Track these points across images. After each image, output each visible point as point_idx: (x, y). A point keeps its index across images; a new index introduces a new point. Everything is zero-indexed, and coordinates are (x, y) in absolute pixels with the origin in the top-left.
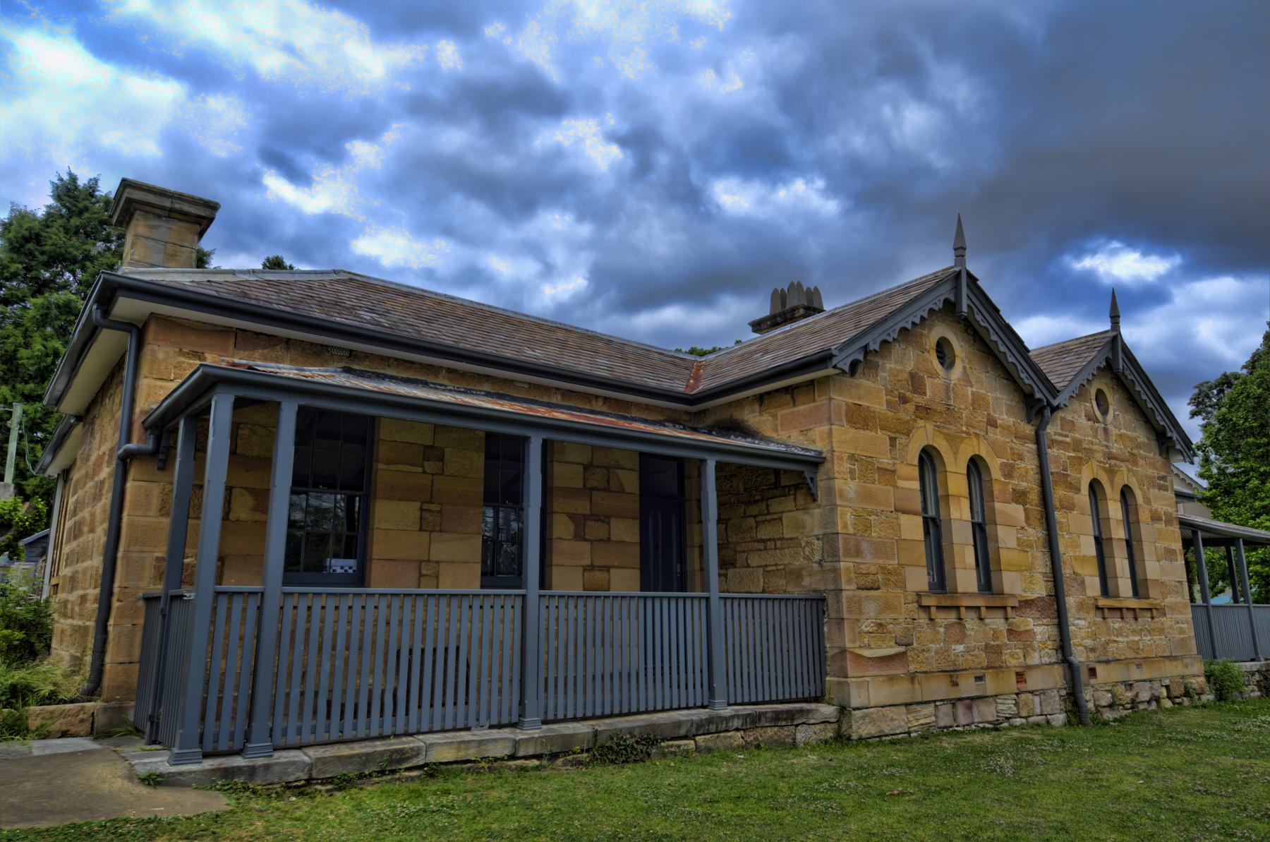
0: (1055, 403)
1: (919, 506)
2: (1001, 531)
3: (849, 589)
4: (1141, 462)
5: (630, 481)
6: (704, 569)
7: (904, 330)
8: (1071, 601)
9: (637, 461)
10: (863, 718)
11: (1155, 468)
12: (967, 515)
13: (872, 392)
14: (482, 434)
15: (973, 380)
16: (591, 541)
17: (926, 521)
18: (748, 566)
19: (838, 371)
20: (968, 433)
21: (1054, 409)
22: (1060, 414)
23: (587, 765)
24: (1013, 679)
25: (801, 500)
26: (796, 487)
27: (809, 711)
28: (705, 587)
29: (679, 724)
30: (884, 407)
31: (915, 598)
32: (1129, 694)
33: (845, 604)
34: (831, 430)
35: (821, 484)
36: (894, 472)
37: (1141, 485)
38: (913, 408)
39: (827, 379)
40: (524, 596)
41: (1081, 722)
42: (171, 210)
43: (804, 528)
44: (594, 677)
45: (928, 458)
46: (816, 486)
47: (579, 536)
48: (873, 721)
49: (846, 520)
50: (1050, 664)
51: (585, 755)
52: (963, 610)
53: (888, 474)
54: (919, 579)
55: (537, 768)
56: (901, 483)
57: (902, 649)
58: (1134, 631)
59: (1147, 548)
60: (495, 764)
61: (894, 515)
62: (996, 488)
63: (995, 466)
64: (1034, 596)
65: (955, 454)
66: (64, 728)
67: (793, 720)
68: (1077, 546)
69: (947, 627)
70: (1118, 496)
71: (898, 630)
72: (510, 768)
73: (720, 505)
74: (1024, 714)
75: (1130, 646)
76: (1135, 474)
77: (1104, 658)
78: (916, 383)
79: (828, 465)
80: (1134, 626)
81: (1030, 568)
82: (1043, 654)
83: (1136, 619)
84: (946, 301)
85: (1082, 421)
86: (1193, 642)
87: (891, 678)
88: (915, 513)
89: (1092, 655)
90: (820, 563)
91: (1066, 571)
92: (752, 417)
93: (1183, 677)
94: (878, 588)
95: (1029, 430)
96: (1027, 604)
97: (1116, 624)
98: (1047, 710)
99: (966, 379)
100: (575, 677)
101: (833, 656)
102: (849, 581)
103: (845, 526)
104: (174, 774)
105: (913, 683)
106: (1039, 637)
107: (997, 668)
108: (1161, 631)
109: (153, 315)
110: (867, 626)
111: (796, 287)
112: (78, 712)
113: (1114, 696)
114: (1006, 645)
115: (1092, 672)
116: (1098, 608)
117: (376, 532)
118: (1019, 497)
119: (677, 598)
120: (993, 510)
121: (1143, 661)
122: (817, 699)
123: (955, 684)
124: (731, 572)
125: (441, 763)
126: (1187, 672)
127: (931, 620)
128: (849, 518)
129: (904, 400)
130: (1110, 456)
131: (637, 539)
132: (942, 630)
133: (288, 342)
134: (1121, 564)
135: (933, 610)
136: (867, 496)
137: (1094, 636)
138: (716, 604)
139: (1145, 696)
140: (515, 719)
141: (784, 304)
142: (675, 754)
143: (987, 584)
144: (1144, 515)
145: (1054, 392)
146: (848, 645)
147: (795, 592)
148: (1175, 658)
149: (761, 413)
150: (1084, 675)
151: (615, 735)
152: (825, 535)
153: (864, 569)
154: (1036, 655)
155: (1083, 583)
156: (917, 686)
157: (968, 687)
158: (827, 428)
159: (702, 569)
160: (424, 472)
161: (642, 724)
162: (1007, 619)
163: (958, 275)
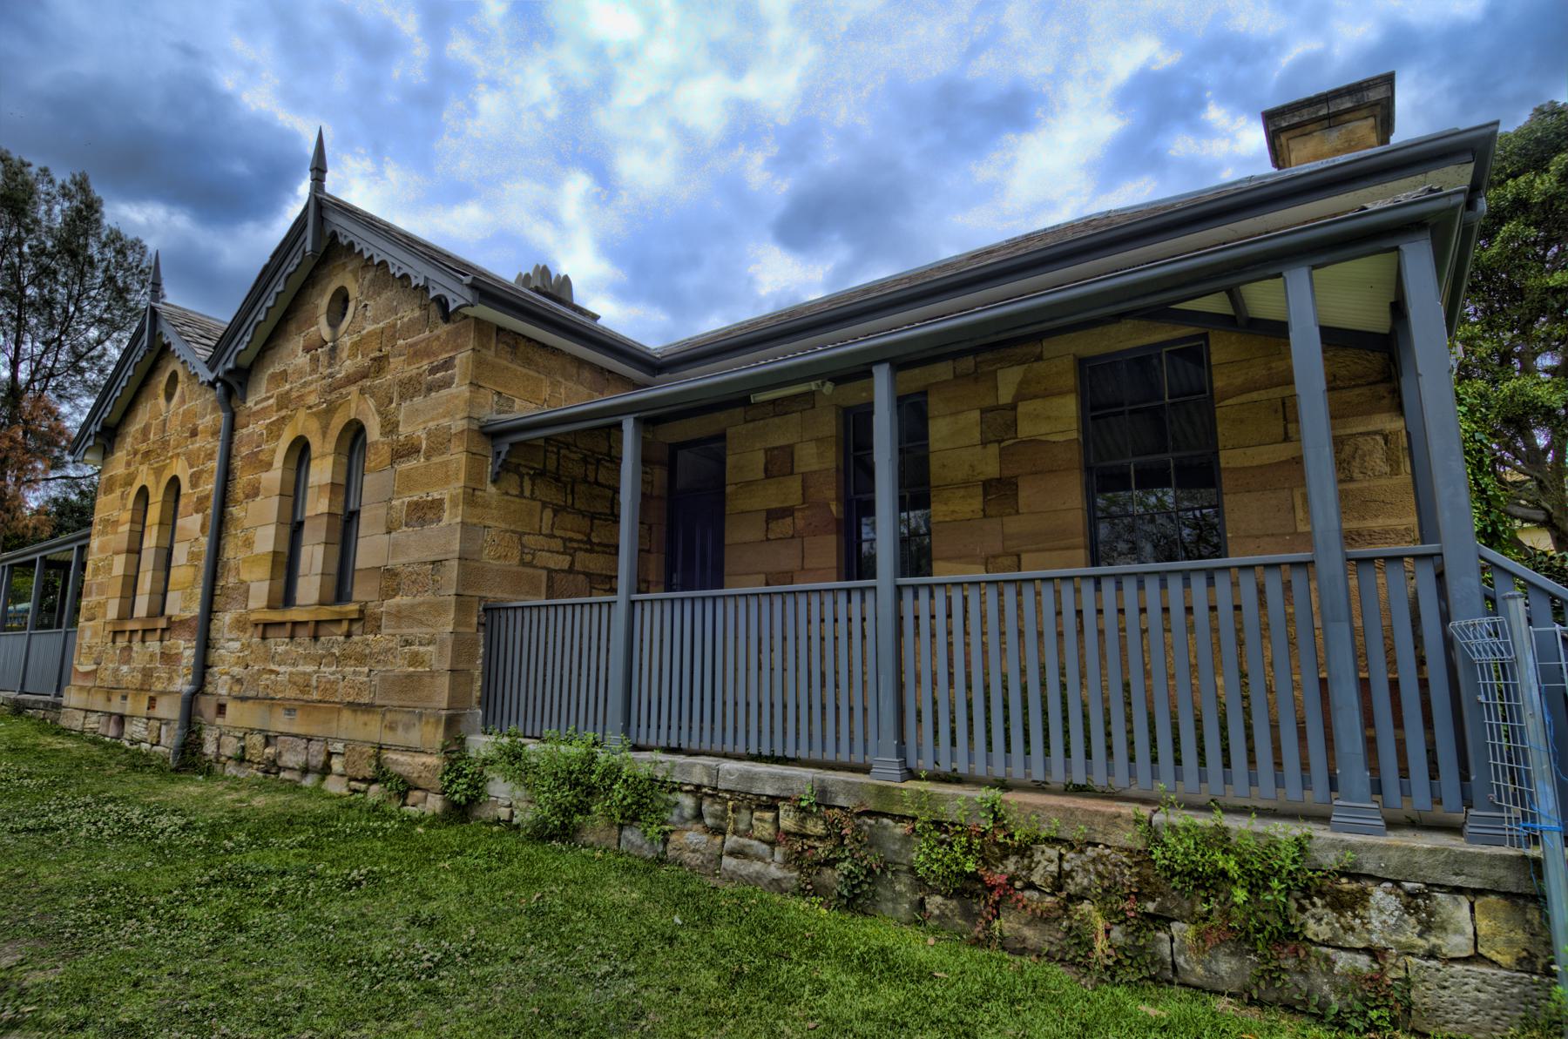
24: (146, 704)
58: (307, 658)
89: (236, 688)
91: (228, 580)
126: (388, 738)
133: (581, 363)
148: (369, 708)
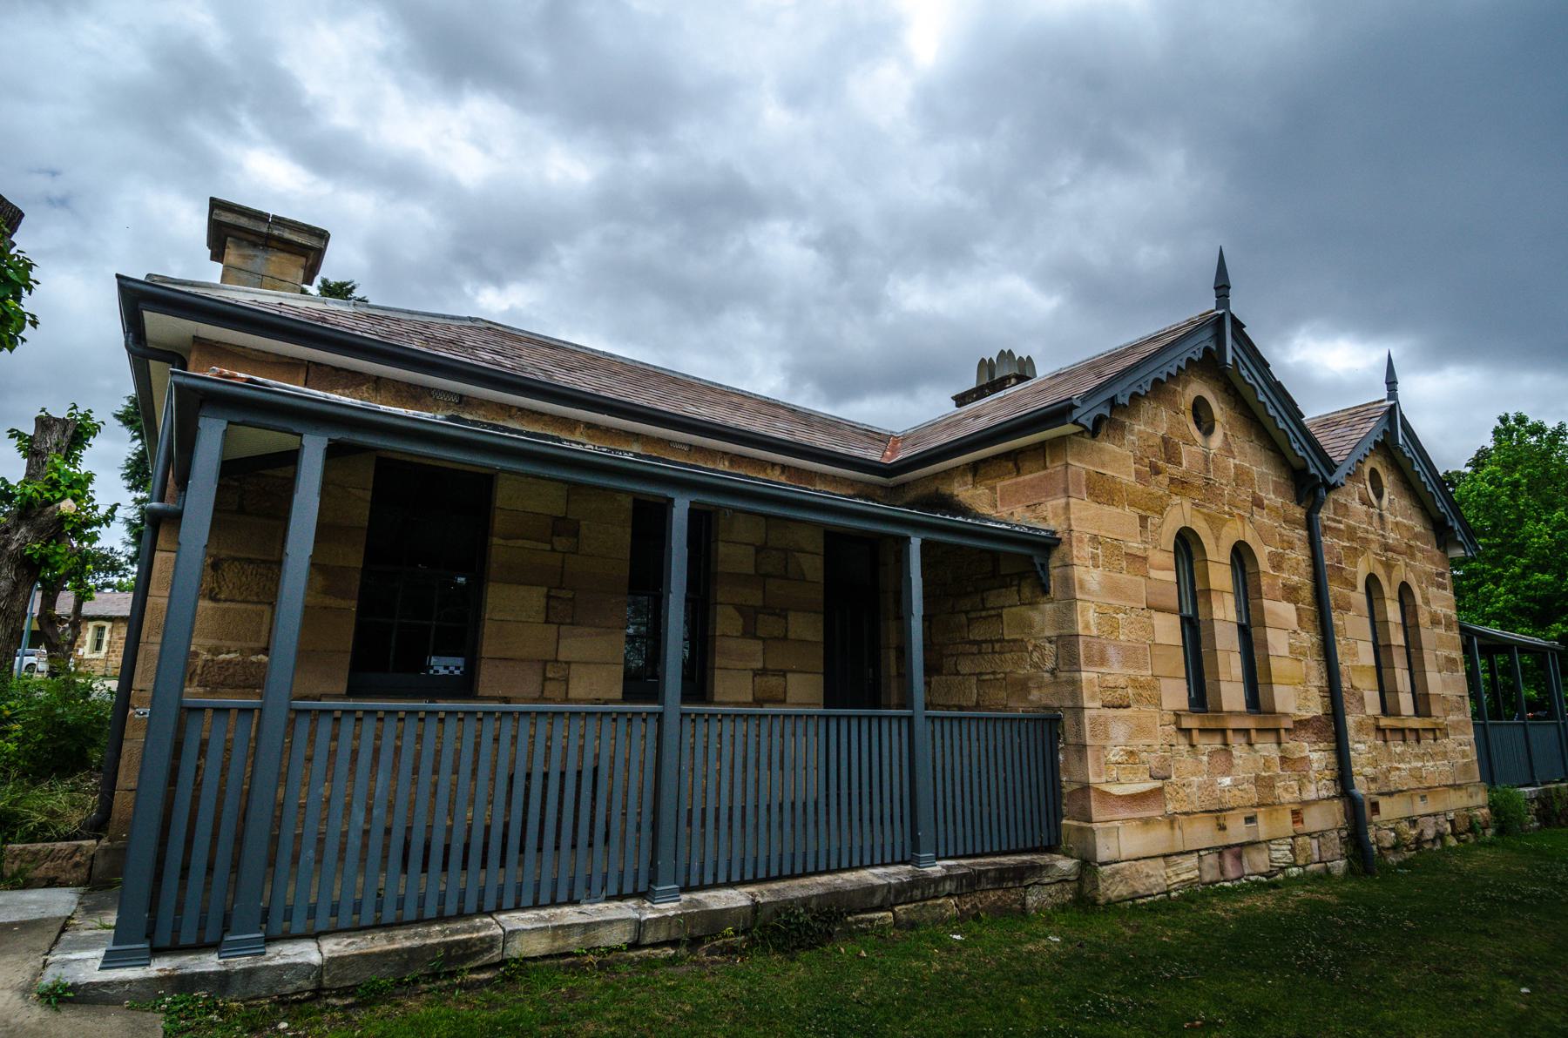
0: (1332, 480)
1: (1175, 604)
2: (1271, 635)
3: (1092, 707)
4: (1419, 555)
5: (813, 567)
6: (905, 676)
7: (1157, 382)
8: (1351, 721)
9: (820, 541)
10: (1112, 875)
11: (1434, 563)
12: (1232, 615)
13: (1117, 459)
14: (627, 502)
15: (1236, 451)
16: (764, 640)
17: (1184, 620)
18: (958, 673)
19: (1077, 429)
20: (1231, 515)
21: (1331, 488)
22: (1333, 496)
23: (742, 953)
24: (1289, 818)
25: (1027, 592)
26: (1021, 576)
27: (1043, 867)
28: (906, 701)
29: (871, 890)
30: (1133, 478)
31: (1173, 718)
32: (1413, 832)
33: (1087, 728)
34: (1068, 504)
35: (1055, 573)
36: (1145, 559)
37: (1419, 582)
38: (1167, 481)
39: (1061, 442)
40: (661, 714)
41: (1368, 871)
42: (269, 237)
43: (1031, 627)
44: (769, 807)
45: (1186, 544)
46: (1047, 574)
47: (749, 633)
48: (1125, 880)
49: (1087, 619)
50: (1328, 798)
51: (741, 938)
52: (1230, 733)
53: (1138, 561)
54: (1176, 694)
55: (670, 961)
56: (1154, 574)
57: (1158, 784)
58: (1417, 757)
59: (1428, 656)
60: (609, 958)
61: (1146, 613)
62: (1265, 582)
63: (1262, 553)
64: (1309, 715)
65: (1217, 539)
66: (51, 874)
67: (1021, 879)
68: (1355, 654)
69: (1211, 755)
70: (1396, 596)
71: (1153, 760)
72: (631, 962)
73: (926, 597)
74: (1301, 862)
75: (1416, 774)
76: (1413, 569)
77: (1385, 790)
78: (1170, 450)
79: (1063, 548)
80: (1416, 750)
81: (1305, 681)
82: (1319, 786)
83: (1418, 741)
84: (1207, 350)
85: (1356, 505)
86: (1476, 766)
87: (1147, 822)
88: (1171, 611)
89: (1373, 786)
90: (1052, 672)
92: (963, 491)
93: (1468, 809)
94: (1128, 706)
95: (1299, 513)
96: (1302, 724)
97: (1398, 748)
98: (1327, 855)
99: (1227, 449)
100: (744, 808)
101: (1070, 794)
102: (1093, 697)
103: (1087, 627)
104: (107, 985)
105: (1172, 828)
106: (1315, 765)
107: (1269, 805)
108: (1445, 755)
109: (198, 341)
110: (1115, 755)
111: (1006, 356)
112: (73, 854)
113: (1398, 835)
114: (1279, 776)
115: (1375, 807)
116: (1378, 729)
117: (488, 624)
118: (1290, 593)
119: (870, 718)
120: (1261, 609)
121: (1426, 792)
122: (1051, 848)
123: (1223, 828)
124: (935, 679)
125: (526, 959)
126: (1471, 803)
127: (1192, 746)
128: (1092, 616)
129: (1156, 471)
130: (1387, 548)
131: (820, 638)
132: (1205, 758)
134: (1402, 677)
135: (1195, 733)
136: (1114, 589)
137: (1375, 763)
138: (921, 725)
139: (1430, 833)
140: (642, 887)
141: (992, 375)
142: (864, 931)
143: (1256, 700)
144: (1424, 619)
145: (1331, 466)
146: (1092, 779)
147: (1019, 708)
149: (974, 485)
150: (1367, 810)
151: (784, 908)
152: (1059, 636)
153: (1110, 681)
154: (1313, 787)
155: (1362, 698)
156: (1177, 831)
157: (1238, 831)
158: (1063, 501)
159: (900, 675)
160: (553, 550)
161: (821, 890)
162: (1279, 744)
163: (1221, 318)
